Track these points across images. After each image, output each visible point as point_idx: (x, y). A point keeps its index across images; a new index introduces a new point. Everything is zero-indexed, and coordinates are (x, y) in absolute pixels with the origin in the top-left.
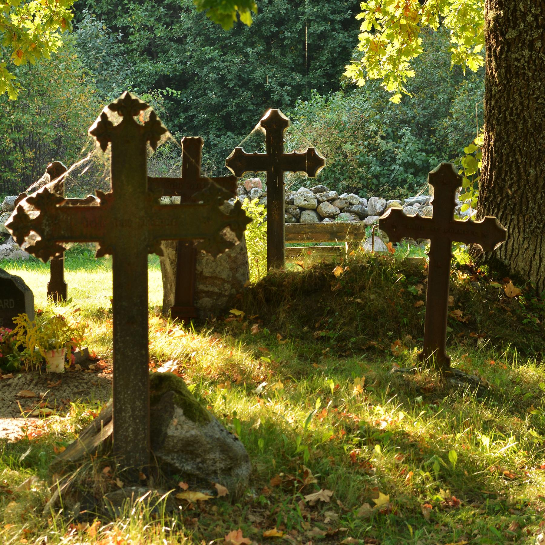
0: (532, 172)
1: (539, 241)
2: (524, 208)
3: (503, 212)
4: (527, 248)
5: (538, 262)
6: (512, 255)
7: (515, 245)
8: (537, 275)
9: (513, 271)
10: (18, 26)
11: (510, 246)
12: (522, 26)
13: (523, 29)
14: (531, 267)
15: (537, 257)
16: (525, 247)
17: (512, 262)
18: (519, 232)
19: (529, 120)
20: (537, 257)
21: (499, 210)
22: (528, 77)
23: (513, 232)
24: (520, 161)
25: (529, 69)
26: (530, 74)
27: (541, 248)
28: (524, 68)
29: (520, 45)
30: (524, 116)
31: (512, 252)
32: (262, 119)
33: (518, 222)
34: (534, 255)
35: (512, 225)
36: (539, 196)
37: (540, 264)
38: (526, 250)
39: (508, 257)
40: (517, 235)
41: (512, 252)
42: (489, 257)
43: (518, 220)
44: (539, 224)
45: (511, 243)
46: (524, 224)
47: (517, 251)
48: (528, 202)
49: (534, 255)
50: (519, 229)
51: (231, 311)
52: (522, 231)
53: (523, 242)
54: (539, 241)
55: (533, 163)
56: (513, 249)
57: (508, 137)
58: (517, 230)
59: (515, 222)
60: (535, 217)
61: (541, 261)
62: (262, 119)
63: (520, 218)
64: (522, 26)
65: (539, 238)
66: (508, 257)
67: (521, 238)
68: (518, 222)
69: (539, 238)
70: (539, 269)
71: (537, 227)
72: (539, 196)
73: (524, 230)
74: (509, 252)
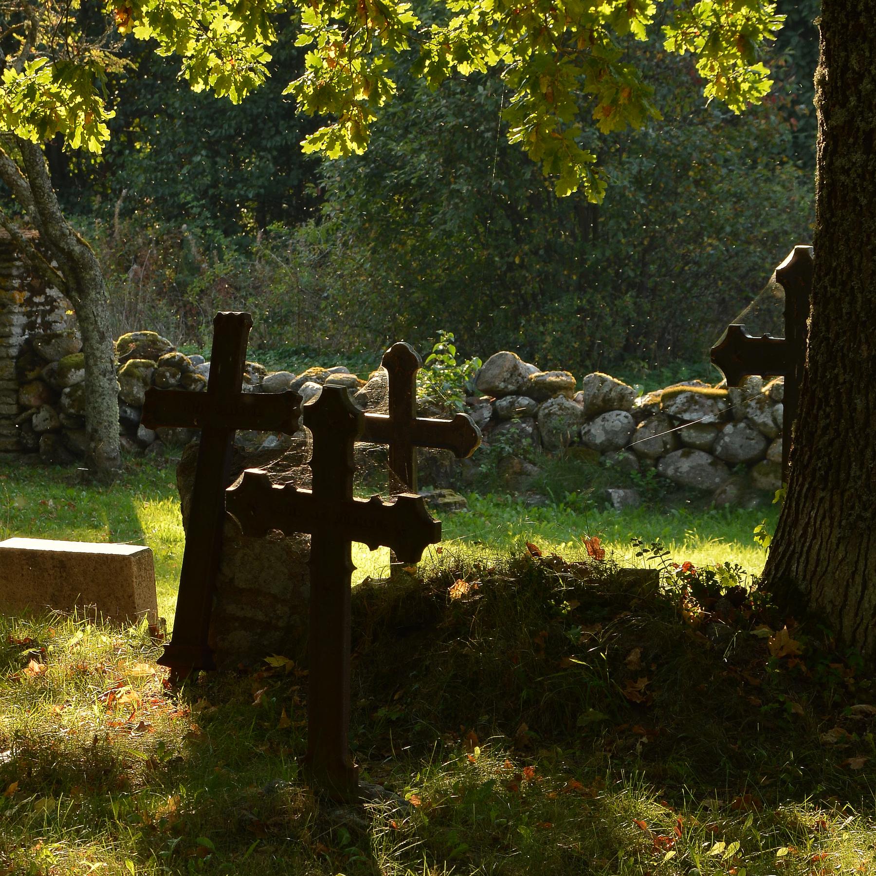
0: (859, 403)
1: (864, 545)
2: (843, 476)
3: (811, 483)
4: (843, 559)
5: (860, 589)
6: (815, 571)
7: (823, 552)
8: (856, 615)
9: (814, 605)
10: (769, 77)
11: (814, 552)
12: (853, 101)
13: (856, 107)
14: (846, 600)
15: (858, 579)
16: (840, 557)
17: (814, 586)
18: (831, 526)
19: (859, 295)
20: (858, 579)
21: (804, 479)
22: (861, 206)
23: (821, 524)
24: (841, 381)
25: (864, 189)
26: (864, 201)
27: (866, 559)
28: (854, 189)
29: (851, 140)
30: (853, 288)
31: (817, 566)
32: (779, 268)
33: (831, 507)
34: (854, 573)
35: (821, 512)
36: (869, 453)
37: (863, 592)
38: (840, 562)
39: (808, 577)
40: (828, 531)
41: (817, 566)
42: (779, 575)
43: (831, 500)
44: (866, 510)
45: (817, 547)
46: (842, 510)
47: (825, 564)
48: (850, 467)
49: (854, 573)
50: (832, 519)
51: (268, 660)
52: (836, 524)
53: (838, 547)
54: (864, 545)
55: (862, 385)
56: (818, 560)
57: (828, 330)
58: (827, 522)
59: (827, 506)
60: (860, 497)
61: (865, 587)
62: (779, 268)
63: (835, 497)
64: (853, 101)
65: (865, 540)
66: (808, 577)
67: (834, 540)
68: (831, 507)
69: (865, 540)
70: (860, 602)
71: (860, 517)
72: (869, 453)
73: (840, 522)
74: (811, 567)
